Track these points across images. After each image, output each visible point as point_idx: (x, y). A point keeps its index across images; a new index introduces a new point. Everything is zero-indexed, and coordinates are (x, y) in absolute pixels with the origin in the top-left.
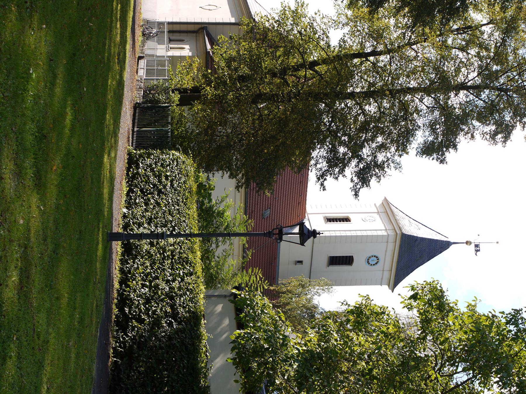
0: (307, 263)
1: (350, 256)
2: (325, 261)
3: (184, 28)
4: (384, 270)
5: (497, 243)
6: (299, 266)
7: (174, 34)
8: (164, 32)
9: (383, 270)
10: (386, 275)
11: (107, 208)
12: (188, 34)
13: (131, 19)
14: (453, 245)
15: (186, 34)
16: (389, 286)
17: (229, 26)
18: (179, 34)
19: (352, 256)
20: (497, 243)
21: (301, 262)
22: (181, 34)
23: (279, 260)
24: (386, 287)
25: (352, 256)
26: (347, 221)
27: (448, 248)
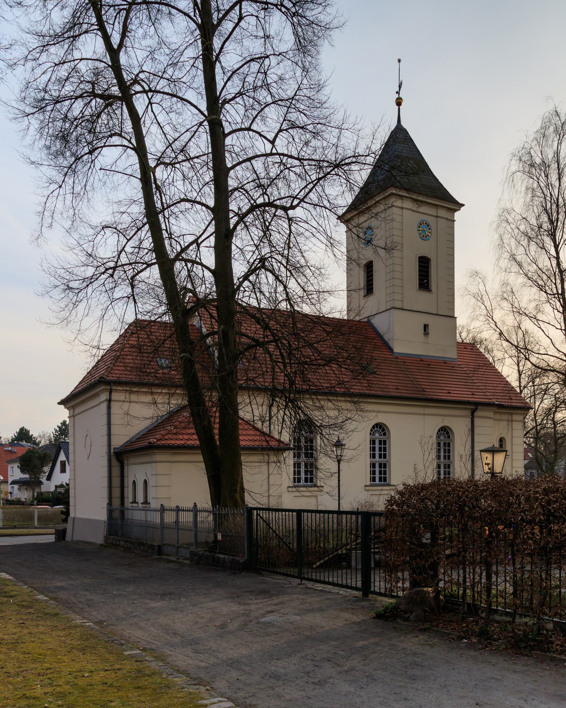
0: (427, 319)
1: (419, 261)
2: (424, 295)
3: (116, 482)
4: (436, 215)
5: (399, 61)
6: (431, 329)
7: (126, 495)
8: (38, 519)
9: (437, 217)
10: (442, 213)
11: (45, 473)
12: (125, 474)
13: (424, 200)
14: (403, 123)
15: (126, 479)
16: (456, 210)
17: (112, 416)
18: (126, 489)
19: (419, 257)
20: (399, 61)
21: (426, 327)
22: (126, 485)
23: (423, 355)
24: (457, 214)
25: (419, 257)
26: (372, 266)
27: (405, 130)
